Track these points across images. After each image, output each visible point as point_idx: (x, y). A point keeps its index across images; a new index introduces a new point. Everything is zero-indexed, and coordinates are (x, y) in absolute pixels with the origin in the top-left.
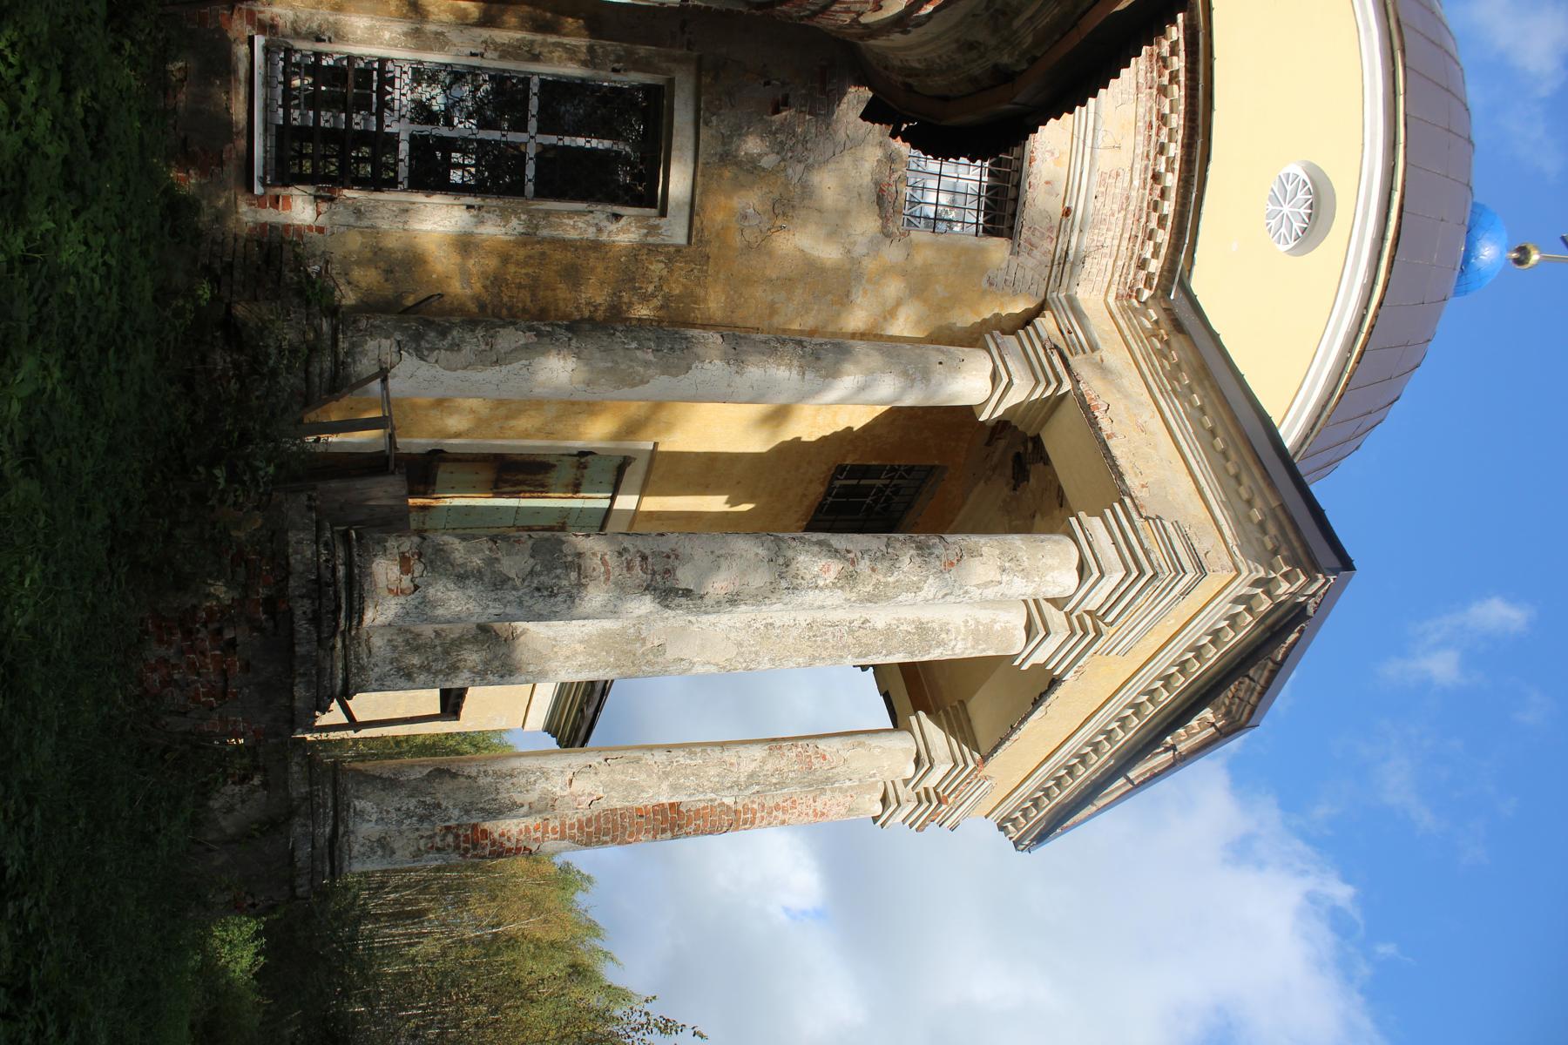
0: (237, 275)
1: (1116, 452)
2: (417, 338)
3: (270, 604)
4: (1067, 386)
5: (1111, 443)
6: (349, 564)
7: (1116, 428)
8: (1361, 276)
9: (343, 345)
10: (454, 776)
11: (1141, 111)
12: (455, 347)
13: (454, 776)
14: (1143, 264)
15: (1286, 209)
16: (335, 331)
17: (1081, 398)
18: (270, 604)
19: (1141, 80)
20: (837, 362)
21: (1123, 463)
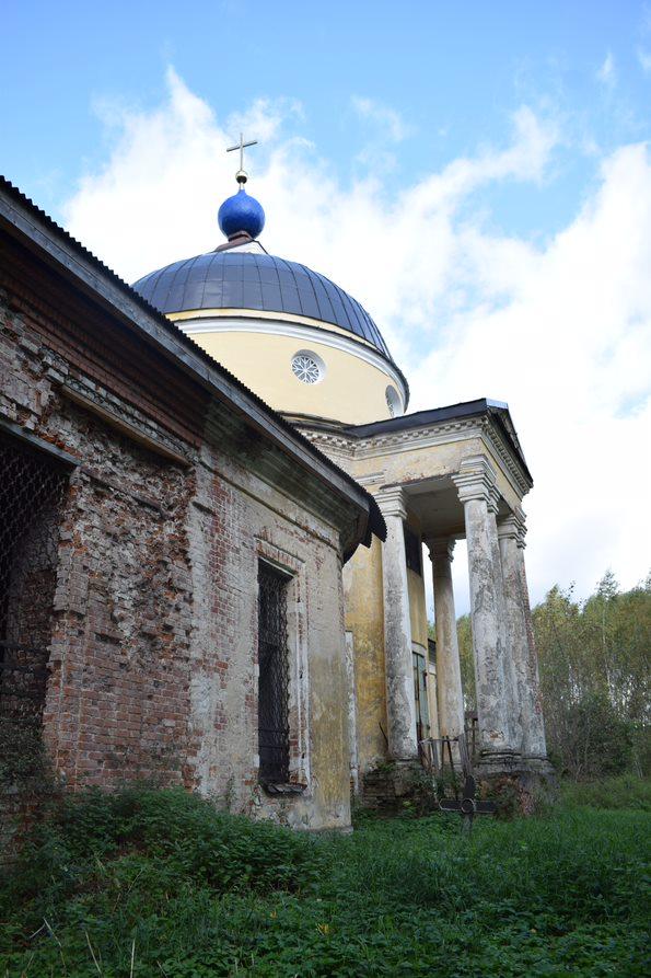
0: (383, 794)
1: (430, 475)
2: (401, 732)
3: (514, 778)
4: (399, 488)
5: (426, 476)
6: (496, 754)
7: (419, 472)
8: (338, 340)
9: (407, 757)
10: (521, 716)
11: (303, 587)
12: (404, 719)
13: (521, 716)
14: (344, 446)
15: (305, 371)
16: (402, 760)
17: (404, 483)
18: (514, 778)
19: (297, 589)
20: (553, 239)
21: (435, 473)
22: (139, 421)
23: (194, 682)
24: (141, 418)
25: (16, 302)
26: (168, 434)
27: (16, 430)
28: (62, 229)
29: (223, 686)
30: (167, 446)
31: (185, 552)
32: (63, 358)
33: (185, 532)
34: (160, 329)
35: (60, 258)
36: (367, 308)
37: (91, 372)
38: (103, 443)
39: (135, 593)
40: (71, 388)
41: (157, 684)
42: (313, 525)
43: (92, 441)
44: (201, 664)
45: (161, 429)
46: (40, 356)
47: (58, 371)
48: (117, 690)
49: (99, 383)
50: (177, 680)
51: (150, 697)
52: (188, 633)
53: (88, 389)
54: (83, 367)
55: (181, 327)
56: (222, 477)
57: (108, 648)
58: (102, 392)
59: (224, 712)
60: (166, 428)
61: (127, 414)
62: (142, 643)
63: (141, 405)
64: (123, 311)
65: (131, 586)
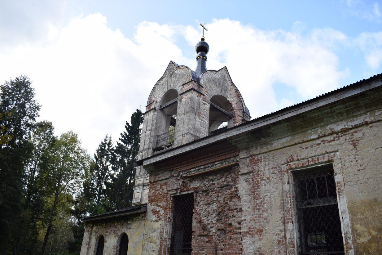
22: (213, 166)
23: (244, 241)
24: (212, 165)
25: (171, 169)
26: (224, 161)
27: (178, 194)
28: (255, 119)
29: (260, 240)
30: (226, 164)
31: (237, 195)
32: (184, 170)
33: (237, 187)
34: (173, 152)
35: (204, 144)
36: (208, 44)
37: (192, 167)
38: (207, 178)
39: (217, 218)
40: (190, 174)
41: (225, 245)
42: (337, 128)
43: (205, 180)
44: (249, 233)
45: (220, 162)
46: (179, 175)
47: (184, 174)
48: (205, 250)
49: (195, 168)
50: (234, 242)
51: (222, 250)
52: (240, 223)
53: (194, 171)
54: (189, 168)
55: (143, 158)
56: (254, 155)
57: (344, 218)
58: (197, 169)
59: (261, 250)
60: (221, 160)
61: (207, 167)
62: (219, 233)
63: (209, 162)
64: (210, 143)
65: (215, 216)
